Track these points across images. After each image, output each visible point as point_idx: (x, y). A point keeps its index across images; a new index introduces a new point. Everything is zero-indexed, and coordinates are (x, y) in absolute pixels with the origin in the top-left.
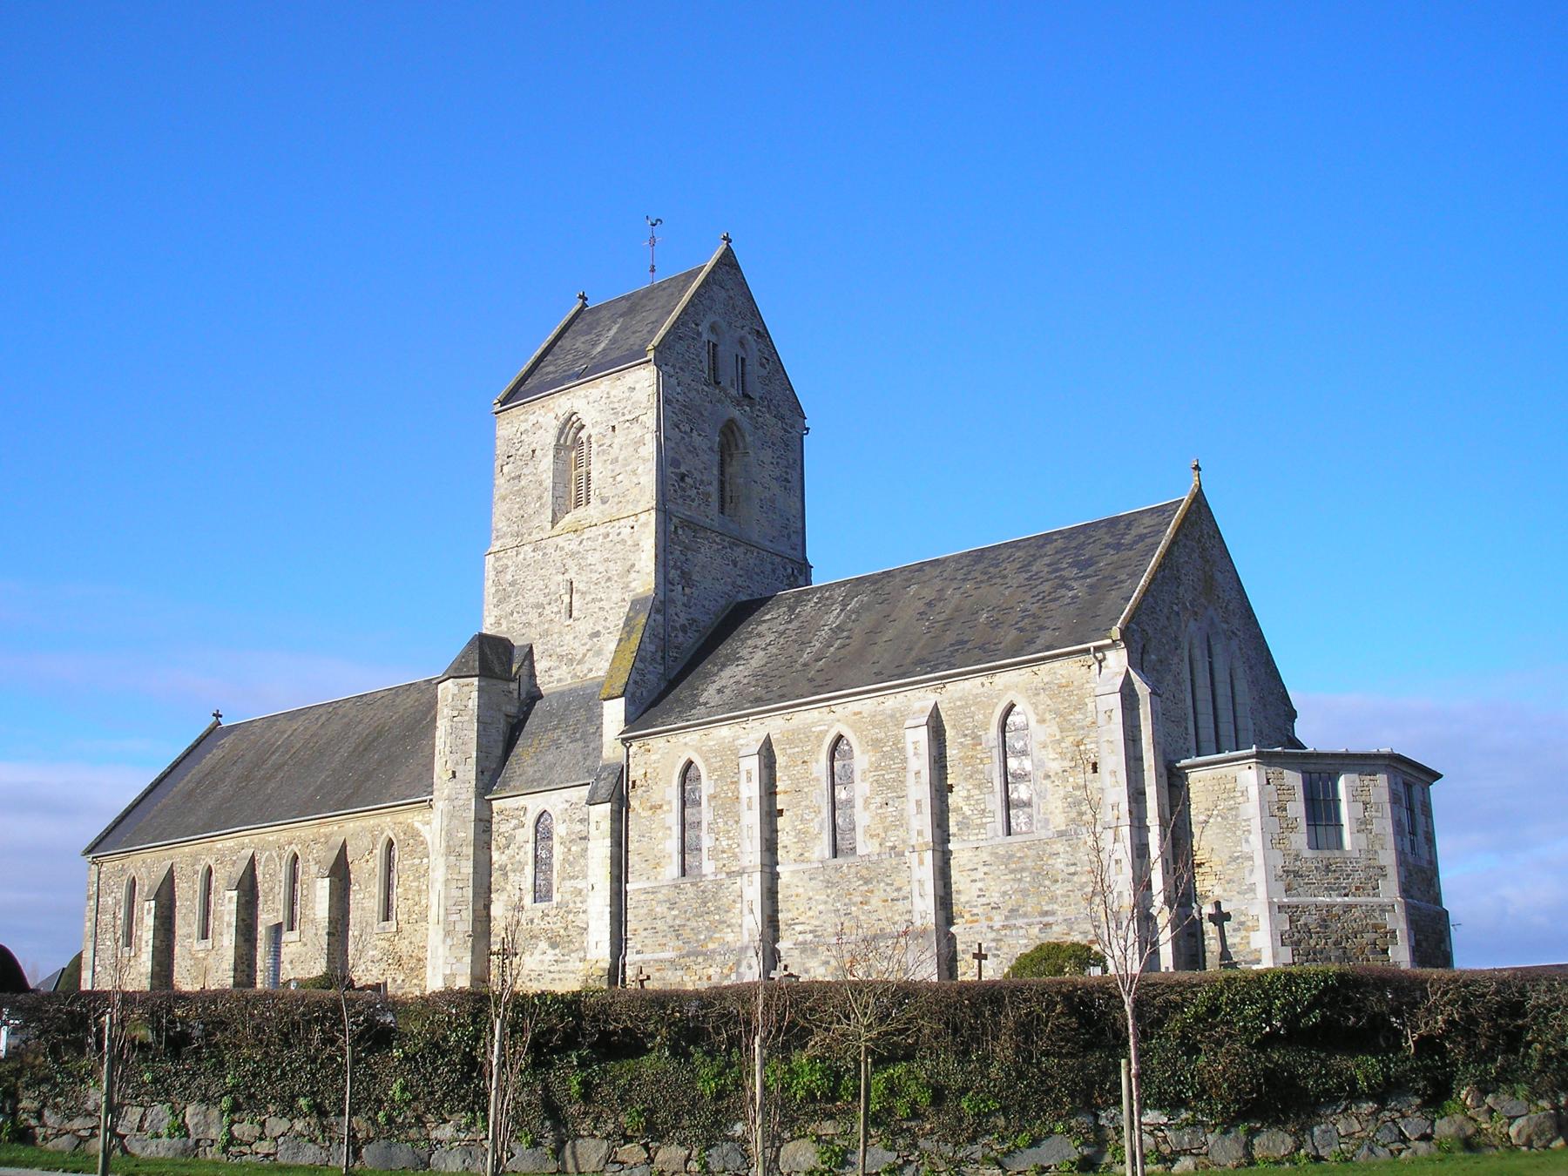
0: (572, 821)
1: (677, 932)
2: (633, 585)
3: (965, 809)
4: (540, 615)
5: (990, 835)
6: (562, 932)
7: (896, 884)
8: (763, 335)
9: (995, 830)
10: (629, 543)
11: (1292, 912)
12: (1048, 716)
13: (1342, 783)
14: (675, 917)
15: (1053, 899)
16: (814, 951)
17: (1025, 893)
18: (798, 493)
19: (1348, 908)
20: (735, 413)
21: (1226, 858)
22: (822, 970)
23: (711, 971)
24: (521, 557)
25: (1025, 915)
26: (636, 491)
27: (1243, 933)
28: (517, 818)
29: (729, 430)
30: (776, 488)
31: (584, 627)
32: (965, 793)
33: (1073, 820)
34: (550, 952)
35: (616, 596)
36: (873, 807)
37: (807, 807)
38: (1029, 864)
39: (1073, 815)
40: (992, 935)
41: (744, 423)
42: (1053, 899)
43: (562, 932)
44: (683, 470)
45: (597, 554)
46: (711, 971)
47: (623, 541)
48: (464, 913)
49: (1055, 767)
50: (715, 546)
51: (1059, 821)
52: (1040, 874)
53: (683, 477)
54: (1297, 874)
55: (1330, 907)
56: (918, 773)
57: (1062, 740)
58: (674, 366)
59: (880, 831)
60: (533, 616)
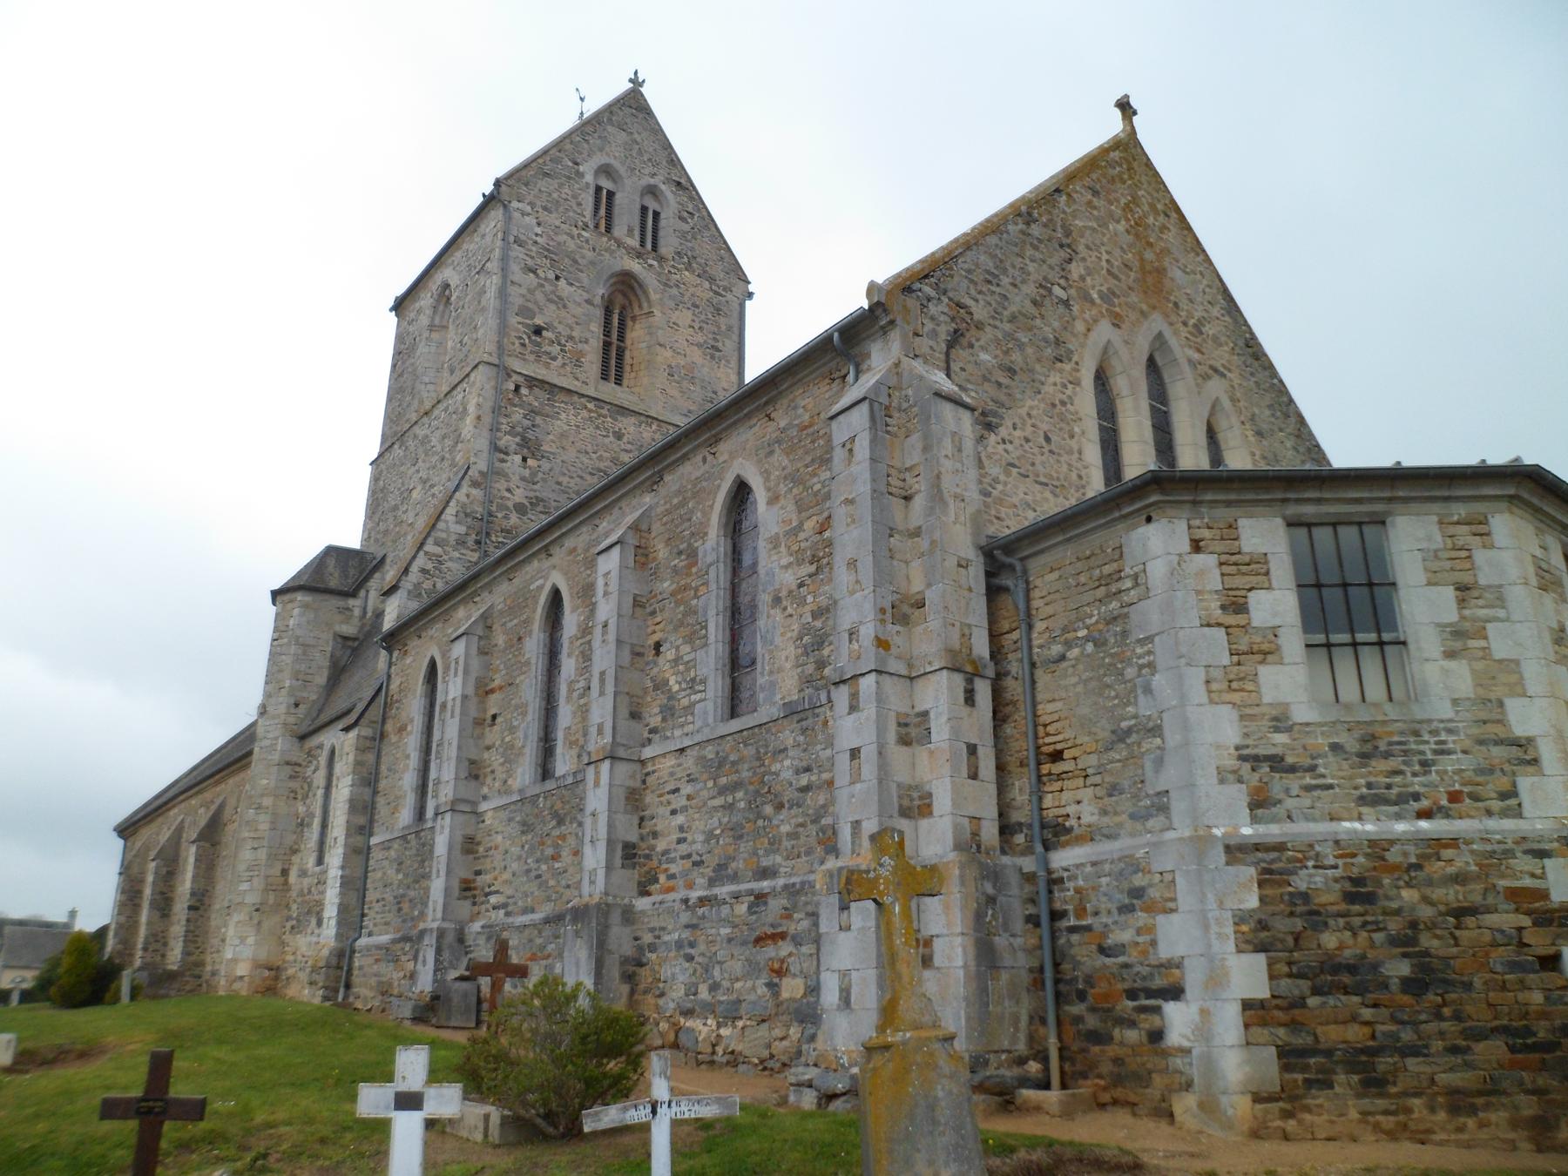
5: (699, 724)
8: (685, 186)
11: (1272, 865)
17: (736, 832)
18: (734, 364)
19: (1437, 845)
20: (635, 266)
21: (1104, 734)
27: (1141, 918)
29: (625, 288)
30: (696, 355)
40: (685, 917)
41: (650, 280)
44: (538, 321)
48: (256, 880)
50: (585, 413)
53: (538, 331)
54: (1276, 763)
55: (1378, 848)
58: (531, 204)
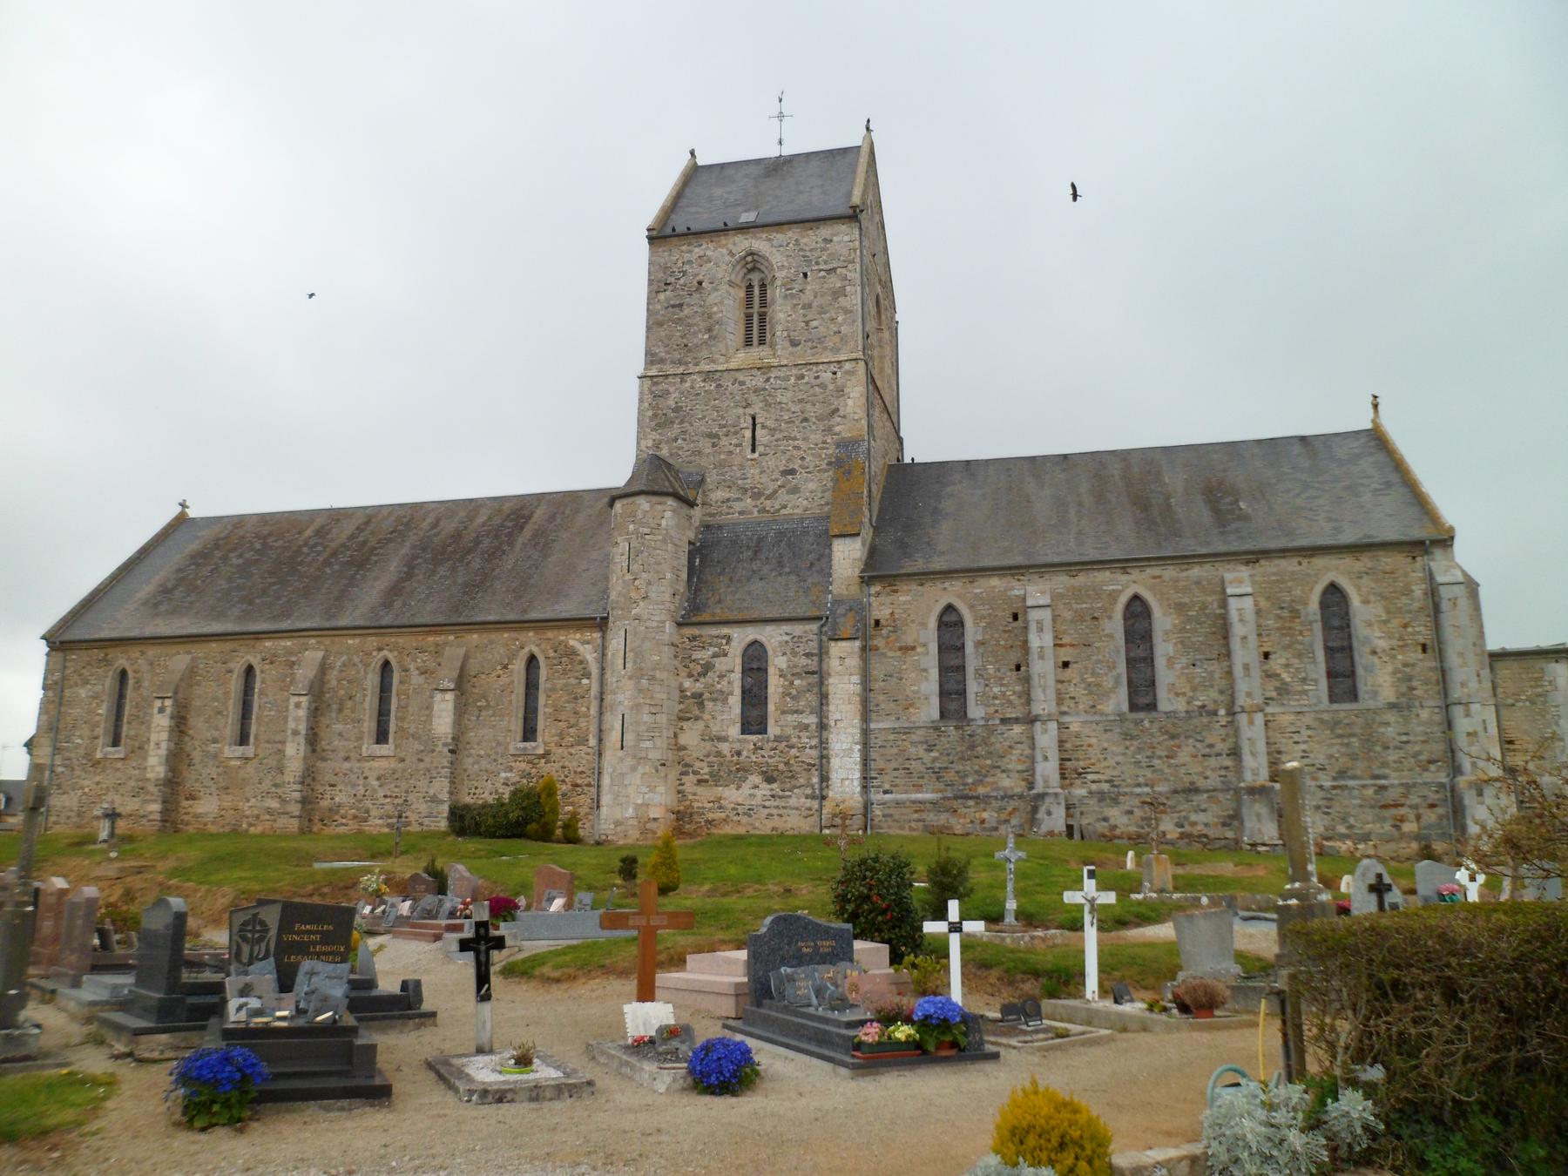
0: (794, 654)
1: (938, 774)
2: (837, 429)
3: (1284, 675)
4: (714, 445)
6: (781, 767)
7: (1209, 740)
9: (1318, 697)
10: (831, 387)
12: (1372, 598)
13: (764, 930)
14: (935, 760)
15: (1385, 764)
16: (1115, 801)
17: (1354, 757)
22: (1125, 820)
23: (985, 815)
24: (688, 384)
25: (1355, 777)
26: (836, 339)
28: (719, 646)
31: (775, 463)
32: (1283, 661)
33: (1403, 695)
34: (764, 785)
35: (816, 437)
36: (1178, 666)
37: (1099, 661)
38: (1357, 730)
39: (1404, 689)
42: (1385, 764)
43: (781, 767)
45: (790, 394)
46: (985, 815)
47: (823, 386)
49: (1382, 644)
51: (1388, 694)
52: (1369, 741)
56: (1244, 638)
57: (715, 656)
59: (1187, 689)
60: (705, 445)
